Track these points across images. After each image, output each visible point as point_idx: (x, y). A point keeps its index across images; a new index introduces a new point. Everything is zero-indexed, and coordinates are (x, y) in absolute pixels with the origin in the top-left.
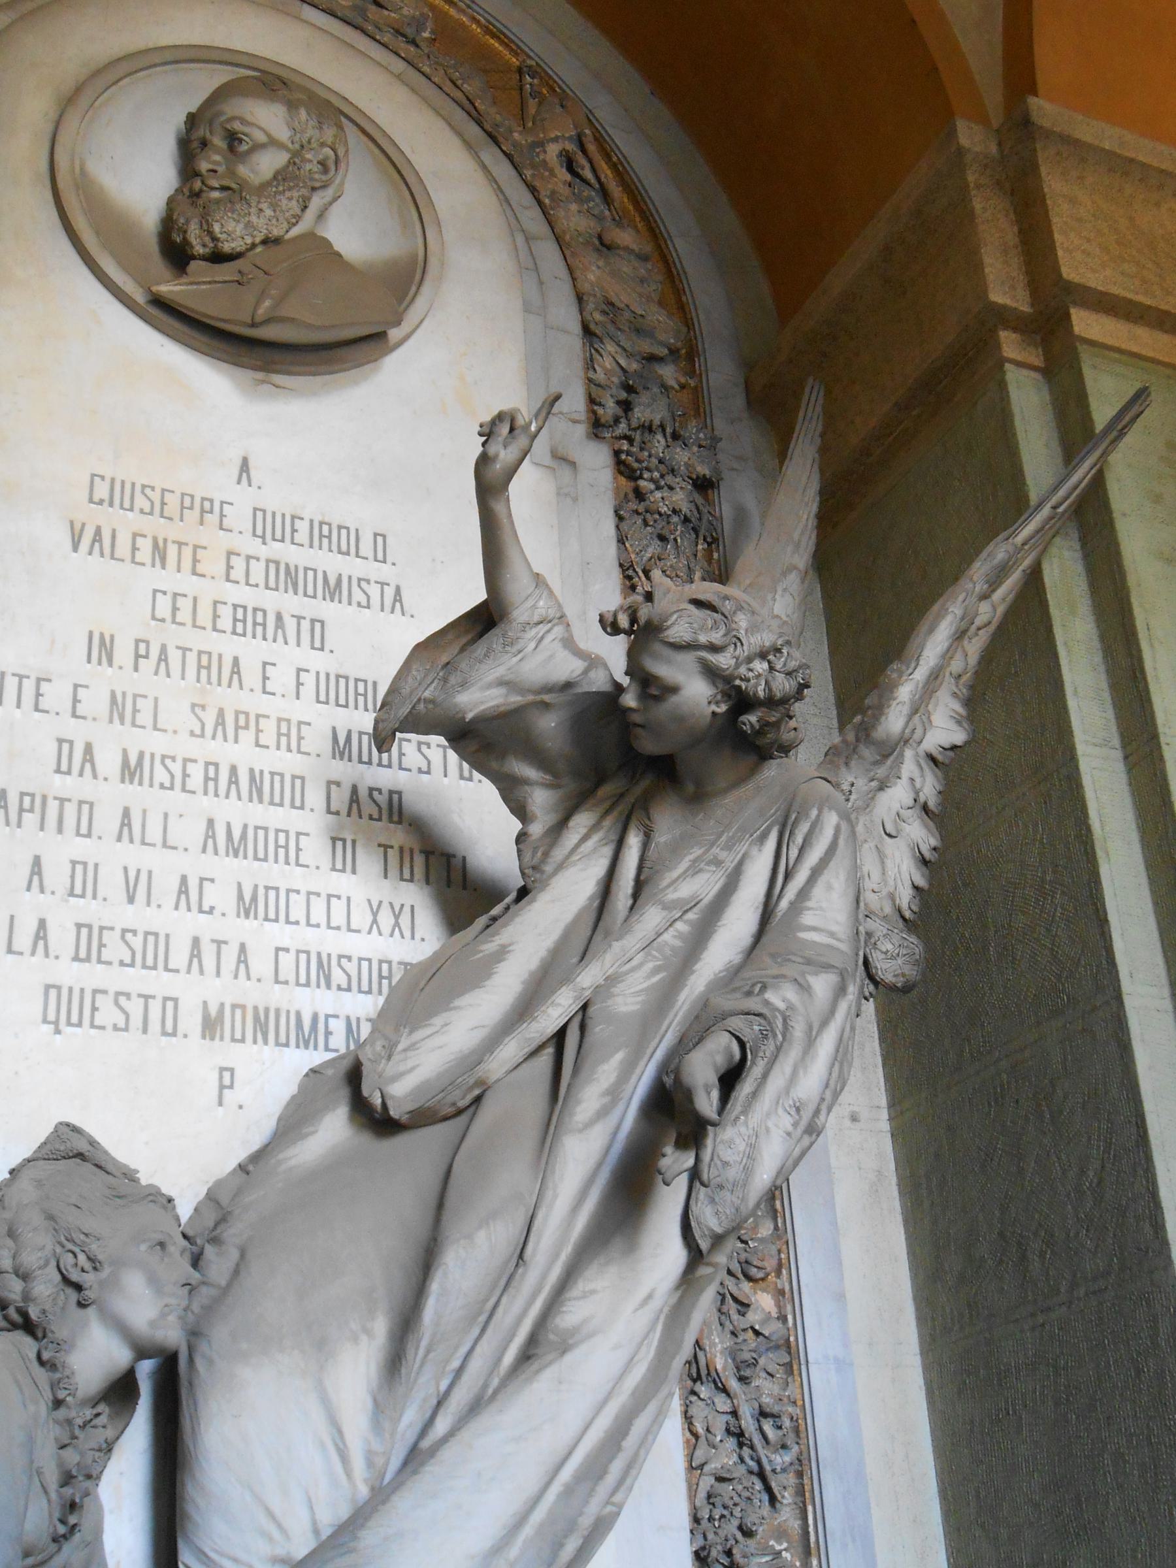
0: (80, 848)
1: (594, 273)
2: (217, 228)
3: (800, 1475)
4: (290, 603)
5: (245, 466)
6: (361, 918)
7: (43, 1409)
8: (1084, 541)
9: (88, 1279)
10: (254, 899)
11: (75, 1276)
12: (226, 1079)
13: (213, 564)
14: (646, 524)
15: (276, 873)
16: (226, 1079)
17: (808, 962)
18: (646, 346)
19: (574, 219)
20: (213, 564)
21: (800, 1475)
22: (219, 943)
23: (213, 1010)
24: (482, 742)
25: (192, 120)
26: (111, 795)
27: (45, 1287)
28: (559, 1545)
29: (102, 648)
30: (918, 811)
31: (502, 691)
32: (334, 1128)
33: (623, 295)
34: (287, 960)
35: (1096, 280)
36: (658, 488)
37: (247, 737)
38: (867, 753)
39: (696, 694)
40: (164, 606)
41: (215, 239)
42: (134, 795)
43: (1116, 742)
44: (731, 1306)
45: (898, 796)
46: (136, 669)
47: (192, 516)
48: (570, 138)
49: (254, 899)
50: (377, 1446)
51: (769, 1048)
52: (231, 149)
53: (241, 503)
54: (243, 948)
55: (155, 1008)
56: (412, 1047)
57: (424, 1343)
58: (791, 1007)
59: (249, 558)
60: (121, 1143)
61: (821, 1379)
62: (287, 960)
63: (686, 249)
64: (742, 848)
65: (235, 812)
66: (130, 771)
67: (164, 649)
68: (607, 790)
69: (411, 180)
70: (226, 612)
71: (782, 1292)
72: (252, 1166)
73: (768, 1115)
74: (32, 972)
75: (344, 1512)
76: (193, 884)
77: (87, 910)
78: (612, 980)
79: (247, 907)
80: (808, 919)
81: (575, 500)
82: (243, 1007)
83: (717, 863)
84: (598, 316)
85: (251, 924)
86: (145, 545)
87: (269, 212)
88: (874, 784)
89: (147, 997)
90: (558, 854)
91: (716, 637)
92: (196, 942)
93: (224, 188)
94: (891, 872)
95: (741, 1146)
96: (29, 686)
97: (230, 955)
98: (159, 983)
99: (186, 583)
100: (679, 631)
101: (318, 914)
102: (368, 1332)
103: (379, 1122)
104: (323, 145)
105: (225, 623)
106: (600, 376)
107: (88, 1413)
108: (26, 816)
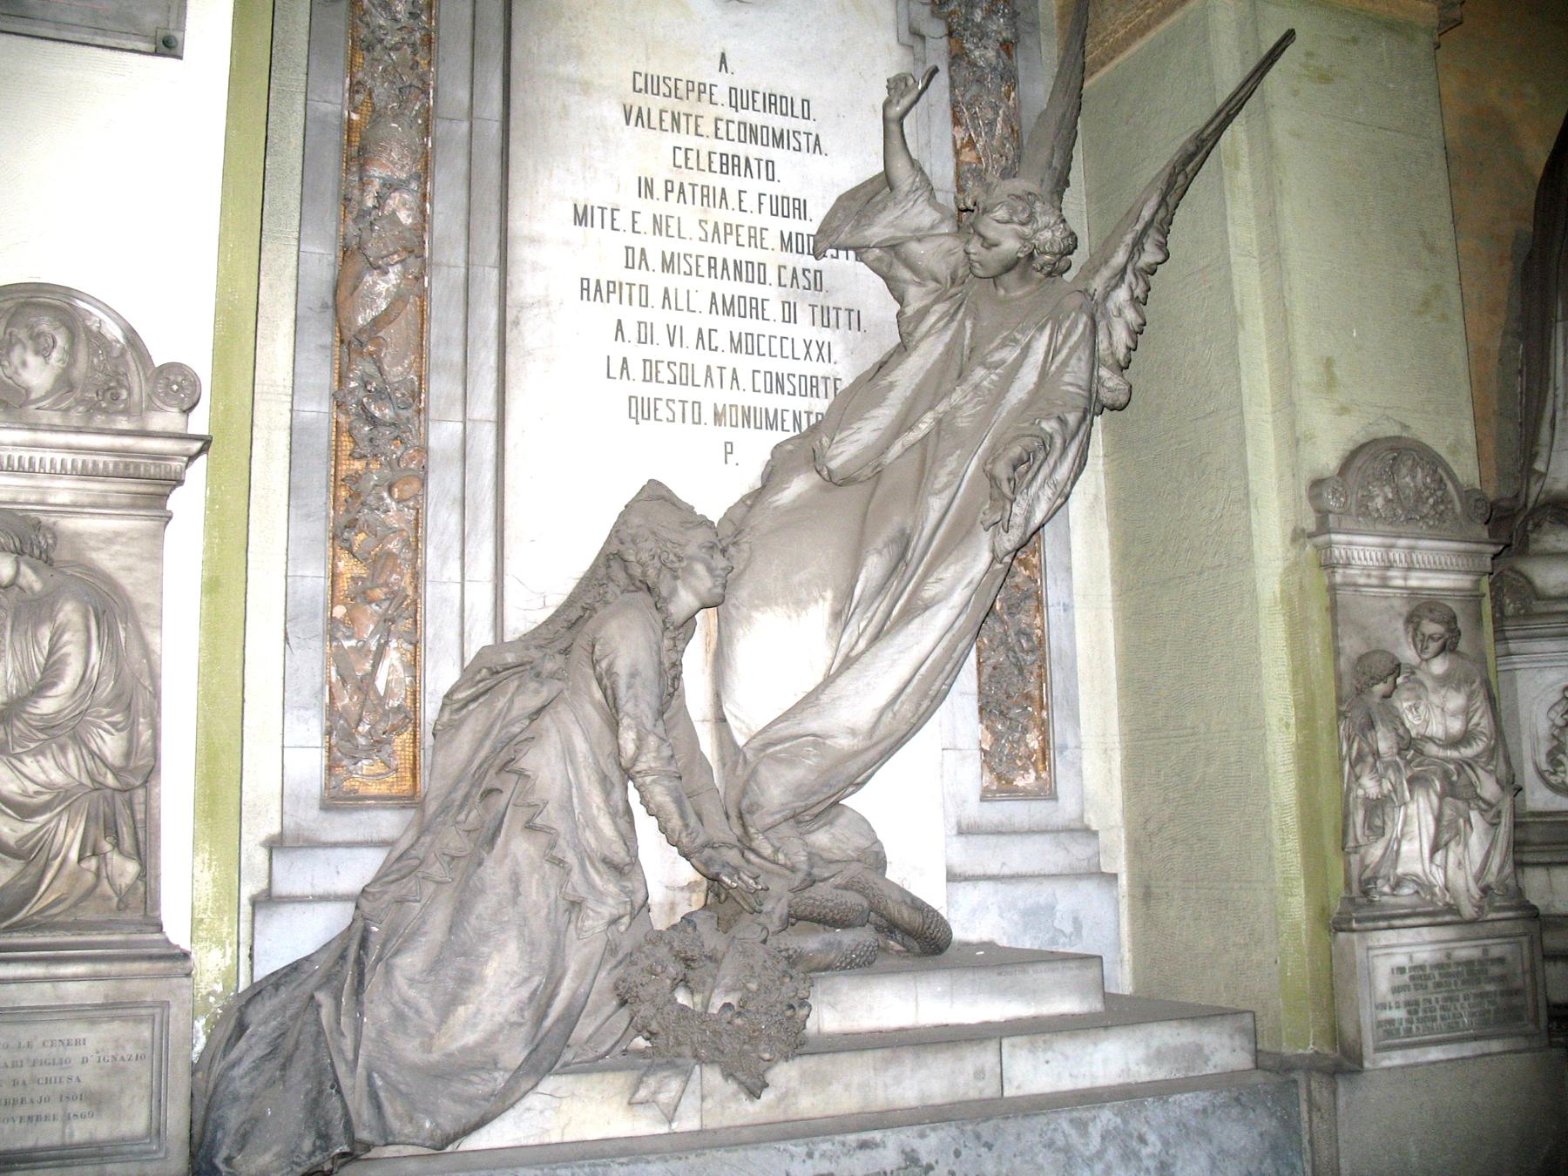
13: (707, 127)
20: (707, 127)
23: (720, 409)
26: (658, 281)
29: (646, 188)
37: (732, 239)
40: (680, 155)
53: (722, 83)
55: (688, 407)
65: (730, 288)
66: (668, 265)
79: (736, 345)
86: (667, 117)
89: (684, 402)
97: (728, 375)
98: (689, 393)
101: (776, 350)
102: (824, 598)
105: (716, 166)
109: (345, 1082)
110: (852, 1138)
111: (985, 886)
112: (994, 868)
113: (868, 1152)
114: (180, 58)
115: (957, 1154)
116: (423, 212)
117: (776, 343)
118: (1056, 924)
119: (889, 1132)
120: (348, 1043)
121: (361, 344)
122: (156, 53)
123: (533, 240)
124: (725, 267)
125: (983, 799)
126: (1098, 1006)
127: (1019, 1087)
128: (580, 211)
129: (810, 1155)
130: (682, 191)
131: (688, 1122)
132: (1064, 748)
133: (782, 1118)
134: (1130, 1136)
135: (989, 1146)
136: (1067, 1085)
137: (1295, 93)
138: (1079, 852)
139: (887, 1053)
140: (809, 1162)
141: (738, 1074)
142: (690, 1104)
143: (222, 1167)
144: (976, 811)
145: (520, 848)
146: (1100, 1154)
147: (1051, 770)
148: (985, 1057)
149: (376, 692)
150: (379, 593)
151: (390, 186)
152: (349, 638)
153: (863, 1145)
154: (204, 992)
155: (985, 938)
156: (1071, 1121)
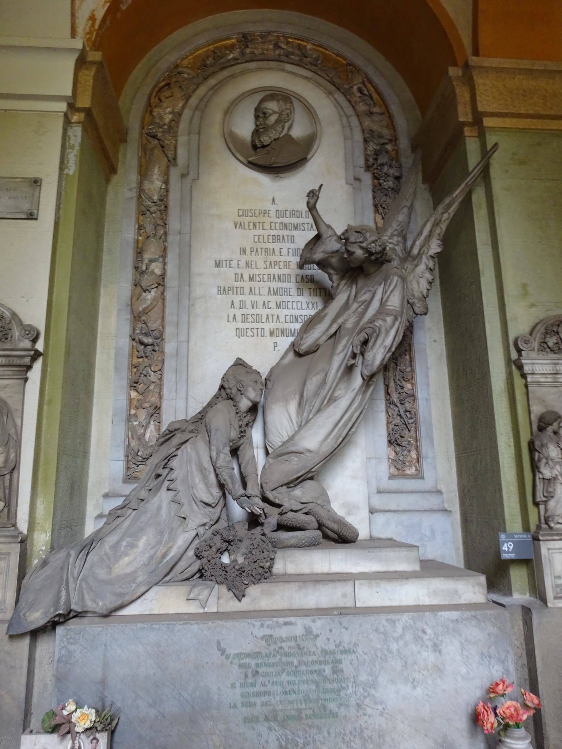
0: (241, 298)
1: (367, 123)
2: (262, 140)
3: (416, 424)
4: (286, 233)
5: (273, 200)
6: (304, 306)
7: (234, 414)
8: (485, 187)
9: (241, 389)
10: (280, 304)
11: (239, 389)
12: (275, 345)
13: (267, 226)
14: (381, 192)
15: (285, 298)
16: (275, 345)
17: (387, 314)
18: (382, 141)
19: (362, 108)
20: (267, 226)
21: (416, 424)
22: (273, 315)
23: (272, 330)
24: (322, 264)
25: (256, 110)
26: (247, 285)
27: (234, 391)
28: (338, 439)
29: (243, 251)
30: (428, 270)
31: (323, 254)
32: (291, 355)
33: (376, 127)
34: (288, 317)
35: (489, 109)
36: (385, 181)
37: (277, 267)
38: (410, 259)
39: (359, 253)
40: (256, 238)
41: (262, 142)
42: (252, 284)
43: (490, 243)
44: (399, 388)
45: (422, 267)
46: (251, 255)
47: (262, 215)
48: (361, 83)
49: (280, 304)
50: (298, 420)
51: (375, 335)
52: (265, 117)
53: (273, 209)
54: (278, 316)
55: (259, 331)
56: (306, 338)
57: (305, 400)
58: (381, 325)
59: (275, 223)
60: (248, 361)
61: (421, 403)
62: (288, 317)
63: (395, 109)
64: (376, 287)
65: (275, 285)
66: (251, 279)
67: (257, 249)
68: (348, 275)
69: (312, 111)
70: (271, 238)
71: (413, 384)
72: (278, 364)
73: (378, 349)
74: (234, 325)
75: (293, 433)
76: (266, 303)
77: (244, 311)
78: (346, 320)
79: (278, 307)
80: (389, 303)
81: (360, 190)
82: (278, 329)
83: (370, 291)
84: (368, 135)
85: (280, 310)
86: (251, 224)
87: (274, 132)
88: (413, 266)
89: (257, 329)
90: (338, 291)
91: (361, 240)
92: (267, 315)
93: (263, 128)
94: (421, 286)
95: (371, 356)
96: (228, 262)
97: (275, 318)
98: (260, 325)
99: (261, 232)
100: (352, 239)
101: (295, 307)
102: (295, 398)
103: (299, 355)
104: (287, 109)
105: (271, 240)
106: (369, 153)
107: (245, 415)
108: (276, 266)
109: (71, 585)
110: (281, 620)
111: (388, 515)
112: (393, 507)
113: (289, 626)
114: (36, 219)
115: (331, 631)
116: (164, 269)
117: (295, 304)
118: (423, 531)
119: (298, 619)
120: (76, 571)
121: (140, 317)
122: (28, 219)
123: (200, 275)
124: (274, 277)
125: (390, 478)
126: (417, 568)
127: (363, 603)
128: (218, 262)
129: (262, 626)
130: (257, 251)
131: (212, 608)
132: (428, 457)
133: (253, 609)
134: (418, 630)
135: (346, 629)
136: (387, 603)
137: (507, 172)
138: (433, 501)
139: (301, 584)
140: (261, 629)
141: (233, 590)
142: (213, 600)
143: (22, 617)
144: (386, 483)
145: (164, 496)
146: (402, 637)
147: (421, 466)
148: (347, 588)
149: (145, 440)
150: (146, 405)
151: (151, 261)
152: (136, 421)
153: (286, 624)
154: (38, 550)
155: (389, 537)
156: (387, 620)
